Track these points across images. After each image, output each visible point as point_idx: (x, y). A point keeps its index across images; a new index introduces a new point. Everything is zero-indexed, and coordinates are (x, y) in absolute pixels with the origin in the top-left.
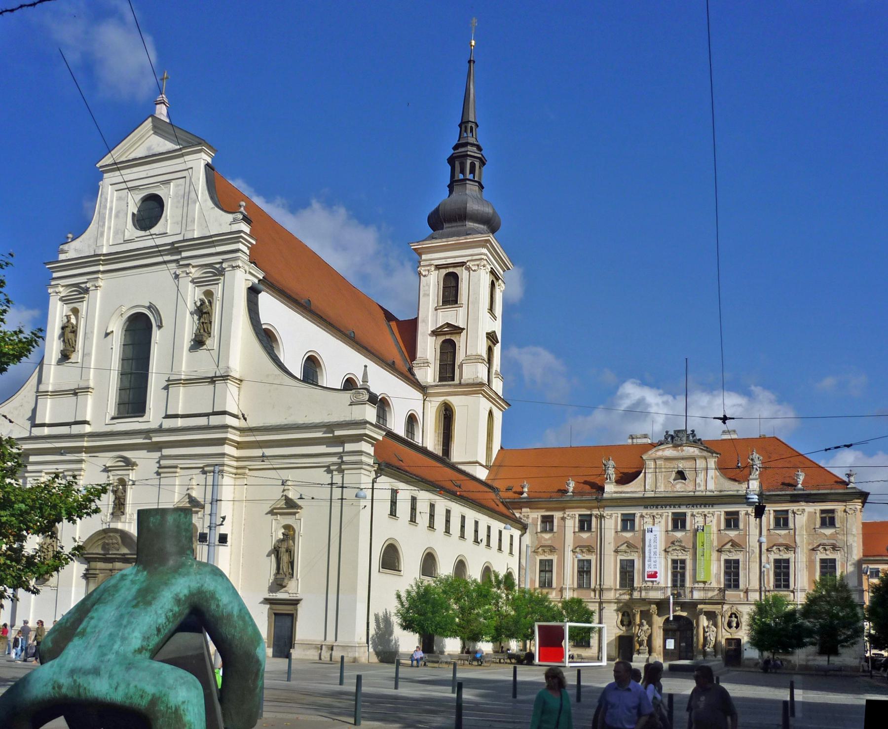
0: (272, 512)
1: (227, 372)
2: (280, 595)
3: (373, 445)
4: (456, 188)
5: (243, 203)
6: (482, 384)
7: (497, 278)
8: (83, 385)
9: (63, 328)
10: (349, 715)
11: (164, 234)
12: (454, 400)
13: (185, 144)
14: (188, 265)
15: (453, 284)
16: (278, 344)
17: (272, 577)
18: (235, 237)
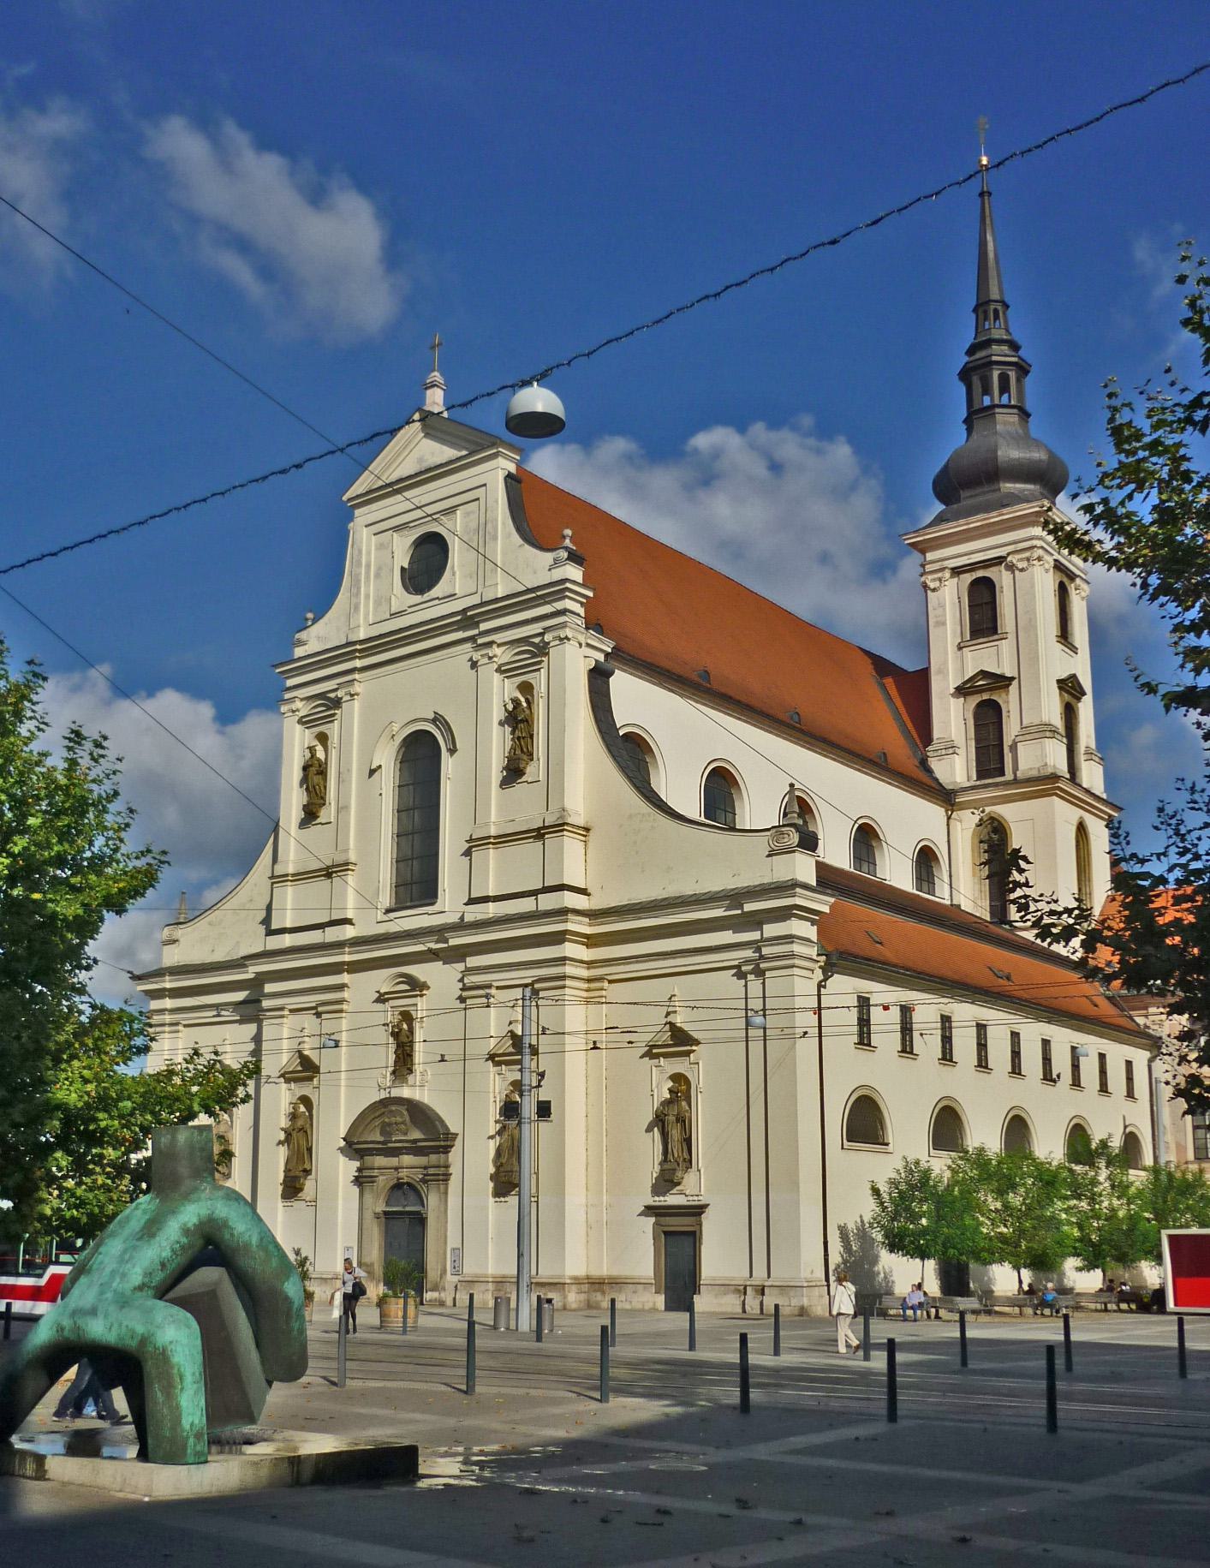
0: (650, 1054)
1: (562, 817)
2: (672, 1199)
3: (813, 922)
4: (978, 425)
5: (568, 532)
6: (1055, 777)
7: (1072, 577)
8: (339, 859)
9: (305, 768)
10: (593, 1388)
11: (451, 596)
12: (1008, 812)
13: (473, 447)
14: (490, 644)
15: (987, 599)
16: (654, 756)
17: (657, 1168)
18: (558, 590)
